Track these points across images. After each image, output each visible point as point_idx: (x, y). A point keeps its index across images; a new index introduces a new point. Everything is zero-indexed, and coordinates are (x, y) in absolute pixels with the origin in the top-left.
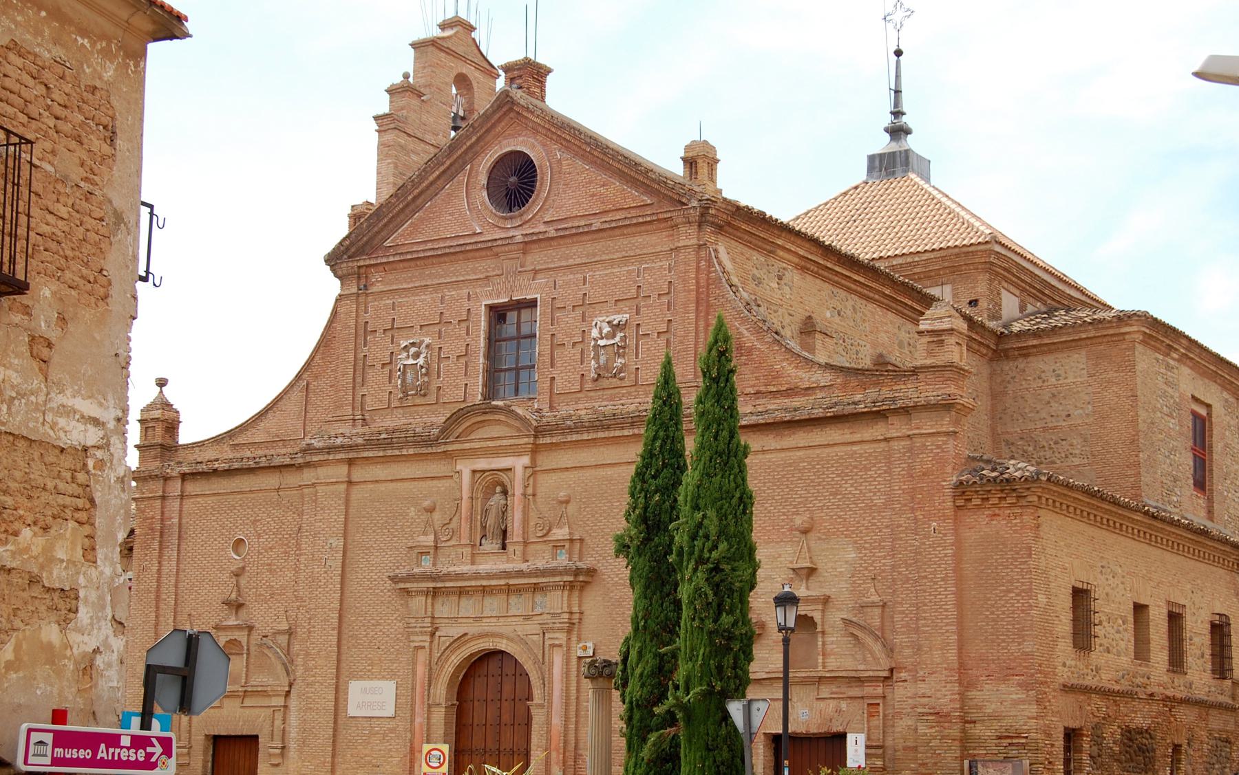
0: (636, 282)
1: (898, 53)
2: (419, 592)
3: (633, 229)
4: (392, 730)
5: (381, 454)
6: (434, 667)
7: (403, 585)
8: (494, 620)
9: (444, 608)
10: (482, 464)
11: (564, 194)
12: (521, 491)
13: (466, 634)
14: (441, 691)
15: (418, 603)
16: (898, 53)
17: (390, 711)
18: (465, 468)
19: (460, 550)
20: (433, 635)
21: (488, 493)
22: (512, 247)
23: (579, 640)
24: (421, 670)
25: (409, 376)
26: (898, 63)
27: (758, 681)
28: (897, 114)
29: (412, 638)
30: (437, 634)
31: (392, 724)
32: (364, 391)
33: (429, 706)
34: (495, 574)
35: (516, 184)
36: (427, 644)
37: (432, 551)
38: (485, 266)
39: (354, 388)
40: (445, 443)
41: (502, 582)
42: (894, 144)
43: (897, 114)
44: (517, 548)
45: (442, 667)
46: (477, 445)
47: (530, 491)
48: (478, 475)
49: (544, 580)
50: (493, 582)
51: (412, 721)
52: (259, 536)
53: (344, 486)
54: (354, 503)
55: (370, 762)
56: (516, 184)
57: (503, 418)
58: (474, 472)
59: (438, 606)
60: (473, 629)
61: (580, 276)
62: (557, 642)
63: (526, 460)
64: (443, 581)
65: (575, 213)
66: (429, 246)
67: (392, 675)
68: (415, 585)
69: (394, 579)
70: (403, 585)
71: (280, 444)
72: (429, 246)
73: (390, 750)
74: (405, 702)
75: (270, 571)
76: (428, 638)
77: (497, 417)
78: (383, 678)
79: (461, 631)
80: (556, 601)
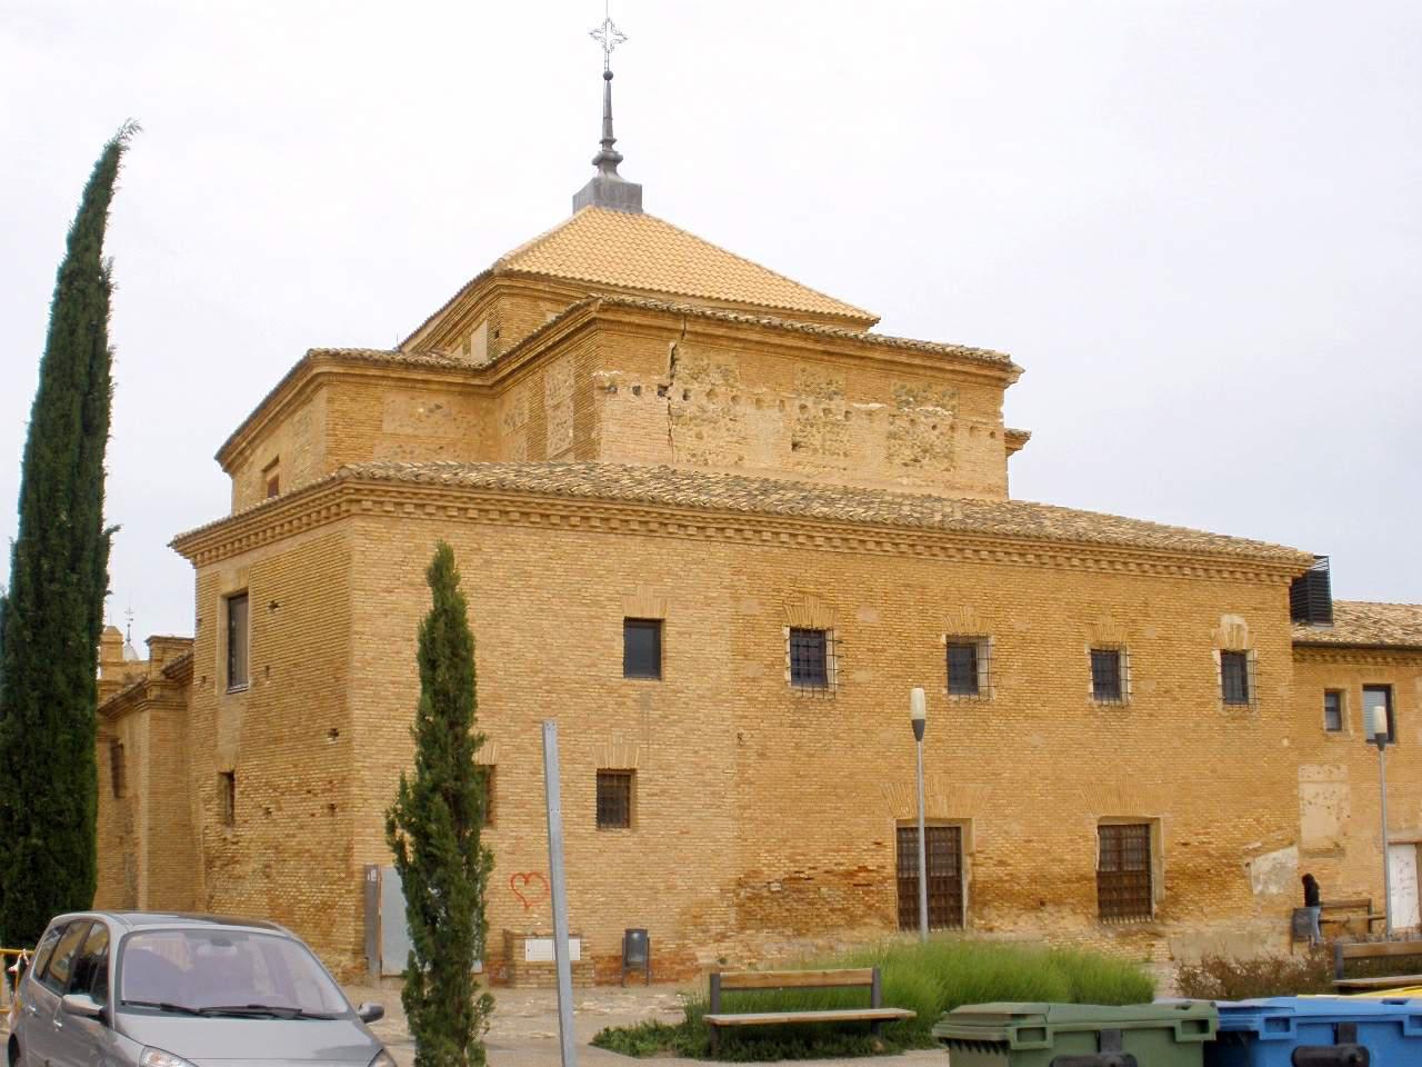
1: (608, 76)
16: (608, 76)
28: (608, 141)
43: (608, 141)
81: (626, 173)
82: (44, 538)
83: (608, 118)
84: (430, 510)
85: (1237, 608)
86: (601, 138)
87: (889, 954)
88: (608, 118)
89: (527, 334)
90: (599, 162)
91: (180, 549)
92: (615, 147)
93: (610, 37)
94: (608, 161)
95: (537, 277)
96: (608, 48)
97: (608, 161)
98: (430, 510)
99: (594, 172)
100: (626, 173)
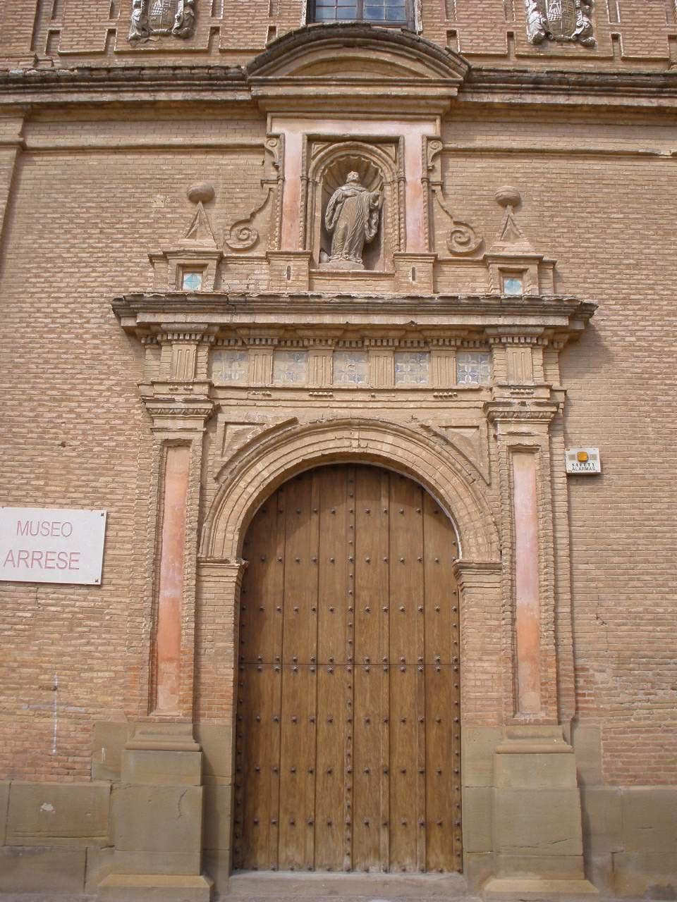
2: (184, 334)
4: (93, 613)
6: (212, 486)
7: (141, 322)
8: (365, 397)
9: (234, 371)
12: (420, 173)
13: (293, 421)
14: (226, 535)
15: (180, 359)
17: (89, 572)
18: (292, 136)
19: (280, 264)
20: (210, 419)
21: (335, 177)
23: (567, 443)
24: (176, 489)
27: (426, 818)
29: (159, 423)
30: (222, 418)
31: (94, 599)
32: (57, 26)
33: (199, 564)
36: (197, 437)
37: (213, 264)
39: (37, 19)
41: (400, 320)
44: (418, 266)
45: (231, 485)
47: (435, 177)
48: (316, 147)
49: (501, 321)
50: (377, 320)
51: (155, 593)
53: (13, 153)
54: (25, 185)
55: (32, 680)
58: (312, 139)
59: (216, 366)
60: (307, 414)
62: (526, 441)
63: (431, 129)
64: (251, 312)
67: (94, 499)
68: (180, 318)
69: (124, 307)
70: (141, 322)
73: (89, 655)
74: (133, 552)
76: (199, 425)
78: (74, 503)
79: (284, 414)
80: (521, 365)
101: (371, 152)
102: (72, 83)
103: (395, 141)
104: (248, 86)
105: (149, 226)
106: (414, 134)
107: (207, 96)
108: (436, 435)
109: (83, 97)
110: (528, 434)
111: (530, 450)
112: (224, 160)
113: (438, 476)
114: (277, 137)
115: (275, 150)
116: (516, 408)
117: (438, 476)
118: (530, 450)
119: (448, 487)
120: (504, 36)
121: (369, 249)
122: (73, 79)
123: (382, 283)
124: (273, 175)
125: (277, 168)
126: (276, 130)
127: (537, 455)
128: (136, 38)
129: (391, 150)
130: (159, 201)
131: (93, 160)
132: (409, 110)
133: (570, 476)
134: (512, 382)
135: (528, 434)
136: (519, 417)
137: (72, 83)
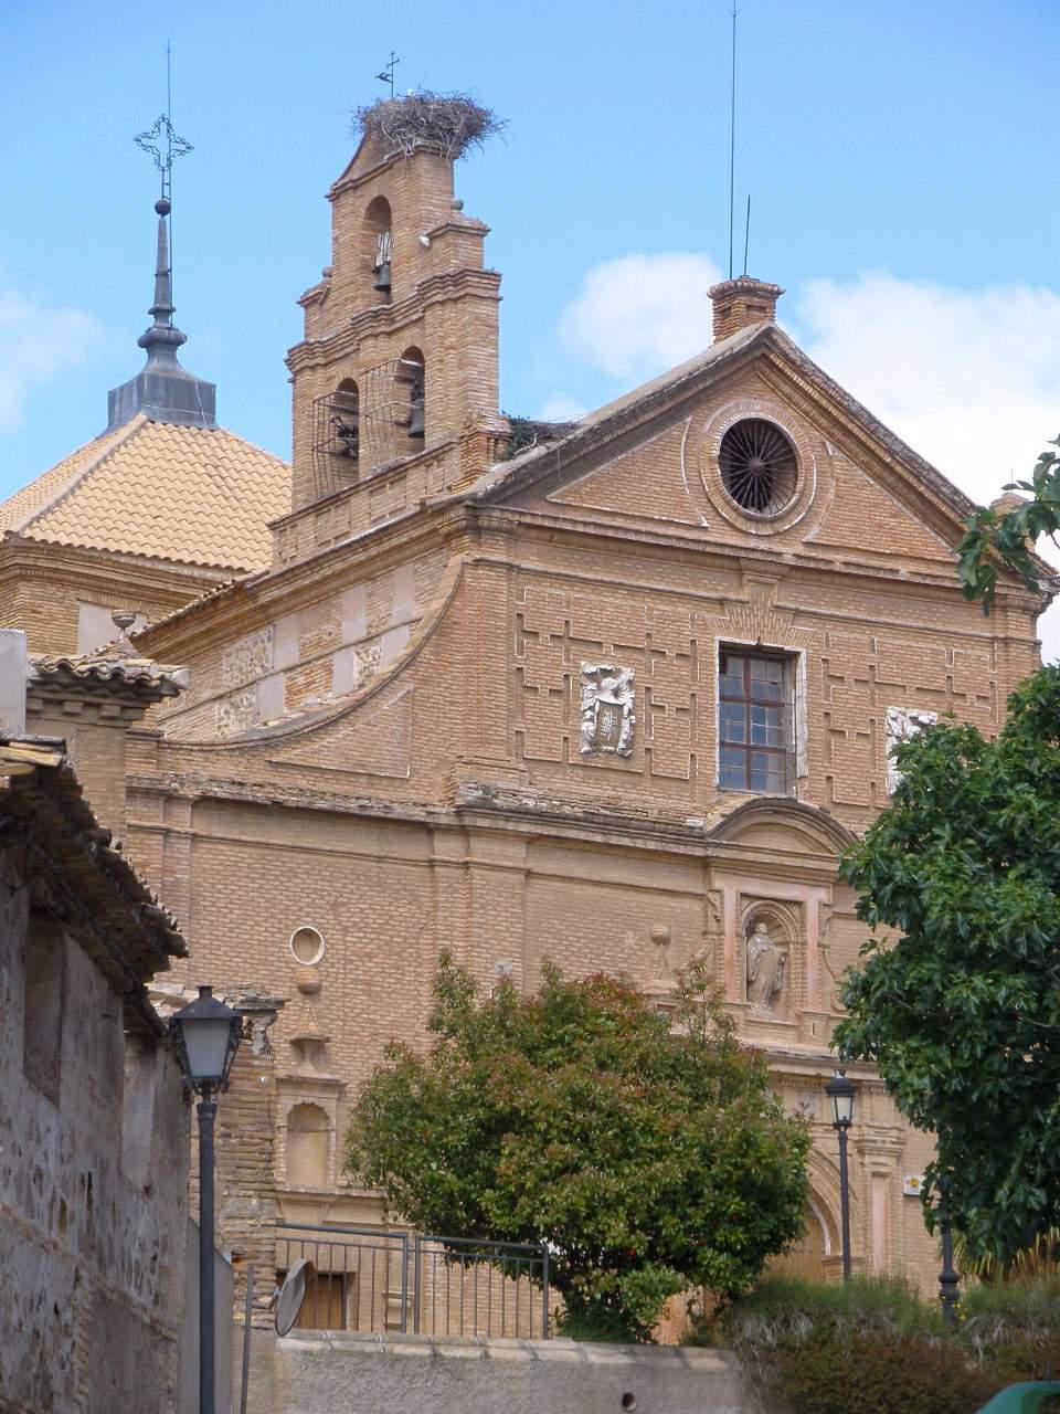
0: (945, 669)
1: (163, 209)
3: (943, 594)
5: (598, 838)
10: (755, 887)
11: (829, 506)
16: (163, 209)
18: (729, 889)
22: (772, 568)
25: (608, 720)
26: (162, 227)
28: (162, 312)
34: (809, 1059)
35: (756, 467)
38: (713, 585)
40: (718, 846)
41: (812, 1071)
42: (156, 363)
43: (162, 312)
44: (817, 1022)
46: (750, 856)
50: (797, 1070)
52: (346, 931)
56: (756, 467)
57: (801, 826)
58: (744, 896)
61: (865, 639)
65: (853, 543)
66: (618, 522)
71: (363, 780)
72: (671, 531)
75: (369, 993)
77: (792, 823)
81: (191, 362)
82: (459, 533)
83: (163, 275)
84: (69, 707)
85: (670, 1290)
86: (151, 305)
87: (155, 1057)
88: (163, 275)
89: (327, 493)
90: (155, 312)
91: (153, 650)
92: (175, 319)
93: (161, 143)
94: (161, 343)
95: (55, 550)
96: (163, 126)
97: (161, 343)
98: (69, 707)
99: (151, 321)
100: (191, 362)
101: (777, 908)
102: (574, 822)
103: (799, 904)
104: (706, 845)
105: (625, 961)
106: (814, 898)
107: (674, 848)
108: (825, 1159)
109: (582, 835)
110: (885, 1165)
111: (883, 1176)
112: (673, 902)
113: (825, 1190)
114: (719, 891)
115: (717, 904)
116: (879, 1145)
117: (825, 1190)
118: (883, 1176)
119: (832, 1199)
120: (868, 787)
121: (773, 996)
122: (577, 819)
123: (515, 876)
124: (713, 926)
125: (718, 921)
126: (718, 884)
127: (888, 1180)
128: (585, 753)
129: (796, 911)
130: (630, 938)
131: (577, 889)
132: (812, 878)
133: (906, 1196)
134: (876, 1124)
135: (885, 1165)
136: (879, 1151)
137: (574, 822)
